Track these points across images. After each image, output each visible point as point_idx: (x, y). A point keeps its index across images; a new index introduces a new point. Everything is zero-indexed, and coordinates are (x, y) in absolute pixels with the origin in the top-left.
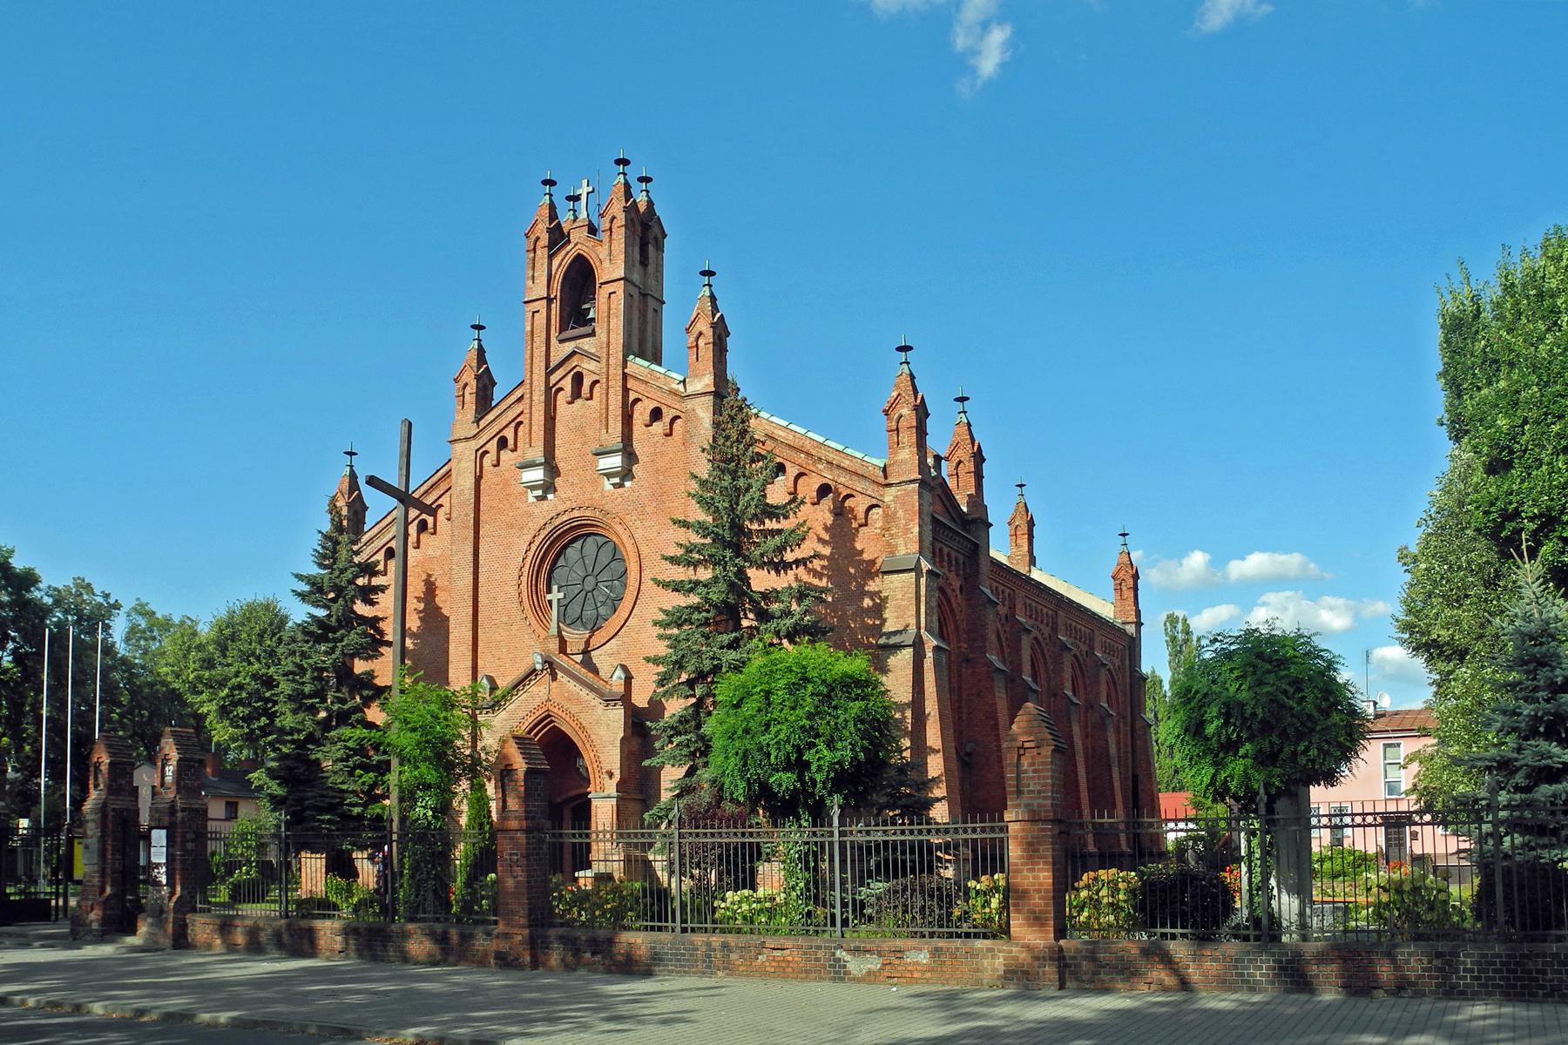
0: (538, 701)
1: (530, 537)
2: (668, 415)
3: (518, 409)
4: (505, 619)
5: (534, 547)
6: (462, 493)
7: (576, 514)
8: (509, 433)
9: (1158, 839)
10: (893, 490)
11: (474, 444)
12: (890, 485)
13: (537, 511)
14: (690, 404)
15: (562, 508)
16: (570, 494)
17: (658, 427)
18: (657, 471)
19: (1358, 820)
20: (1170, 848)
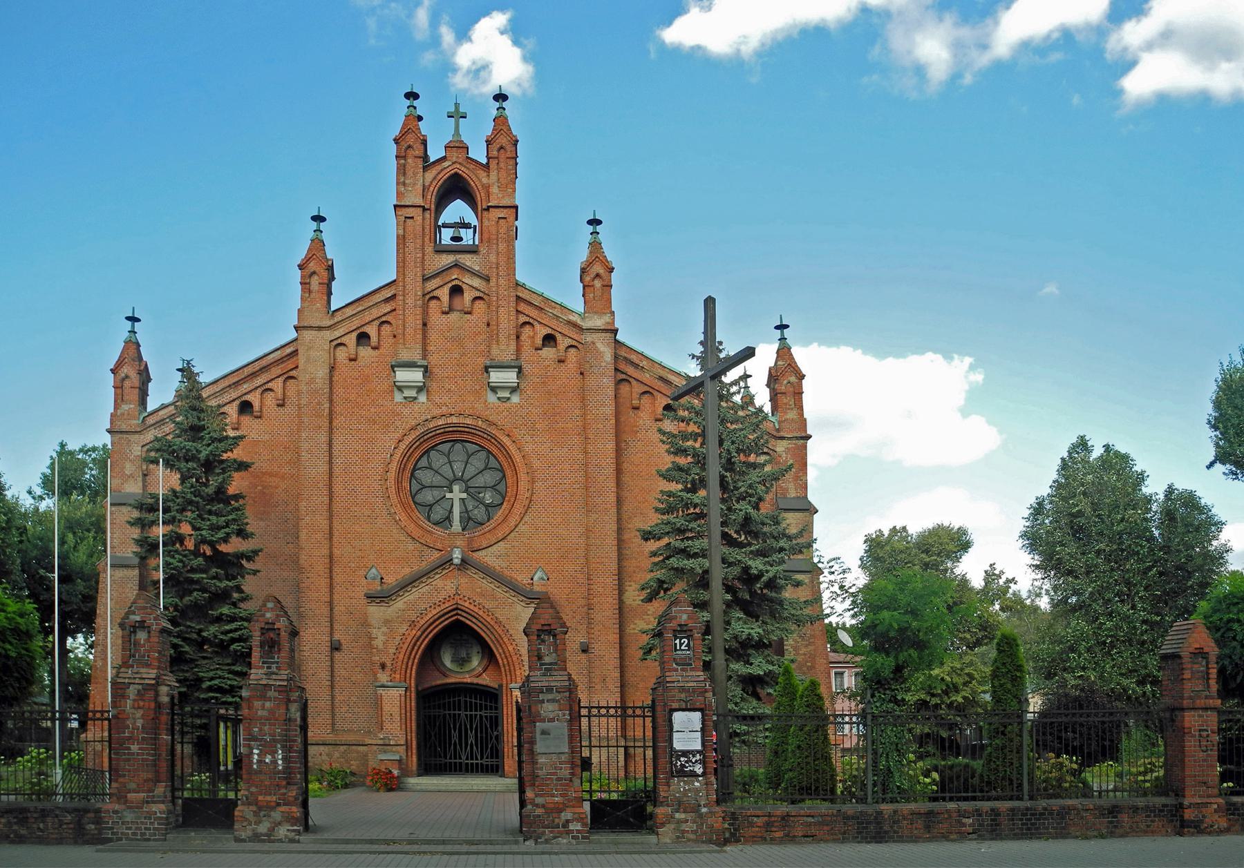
0: (443, 595)
1: (398, 435)
2: (563, 343)
3: (387, 308)
4: (367, 513)
5: (403, 446)
6: (311, 381)
7: (454, 420)
8: (372, 331)
9: (959, 704)
10: (785, 443)
11: (329, 335)
12: (782, 438)
13: (406, 411)
14: (589, 338)
15: (437, 412)
16: (446, 399)
17: (548, 352)
18: (549, 393)
19: (98, 715)
20: (699, 374)
